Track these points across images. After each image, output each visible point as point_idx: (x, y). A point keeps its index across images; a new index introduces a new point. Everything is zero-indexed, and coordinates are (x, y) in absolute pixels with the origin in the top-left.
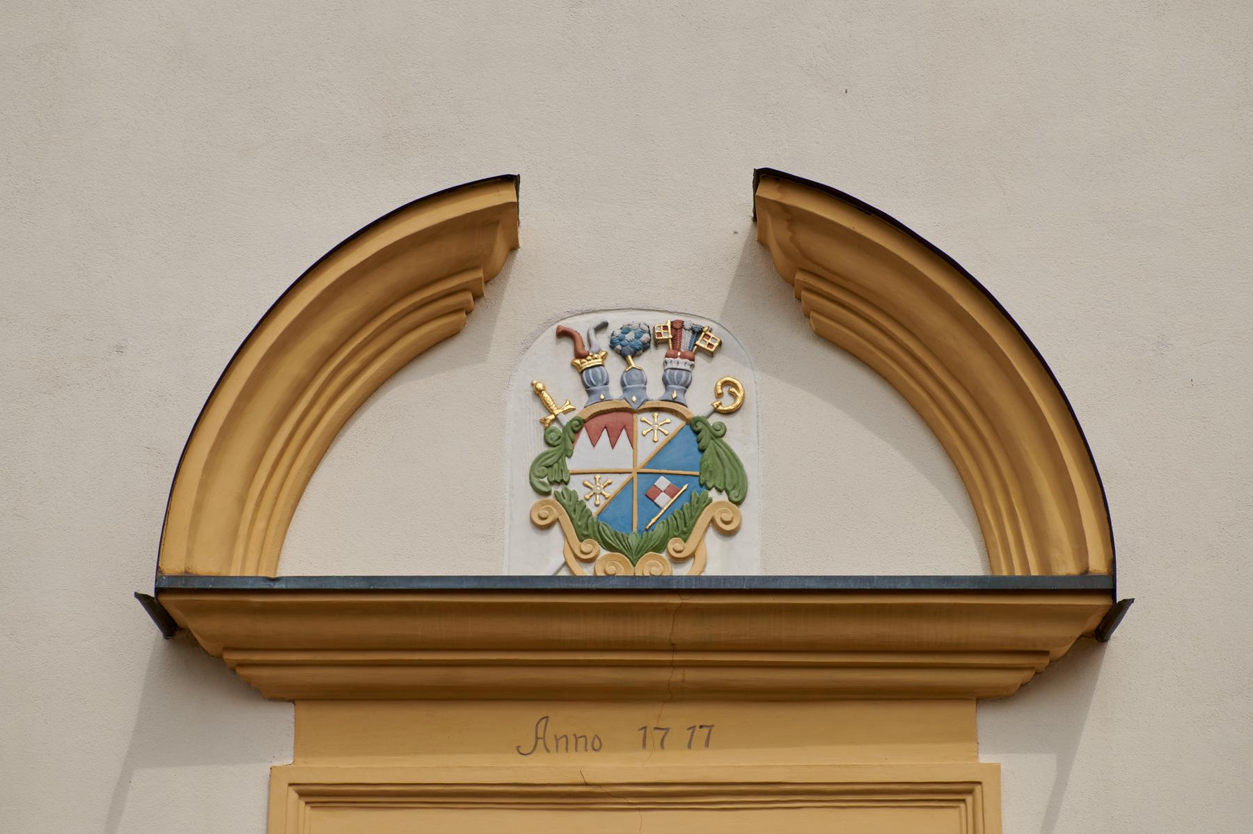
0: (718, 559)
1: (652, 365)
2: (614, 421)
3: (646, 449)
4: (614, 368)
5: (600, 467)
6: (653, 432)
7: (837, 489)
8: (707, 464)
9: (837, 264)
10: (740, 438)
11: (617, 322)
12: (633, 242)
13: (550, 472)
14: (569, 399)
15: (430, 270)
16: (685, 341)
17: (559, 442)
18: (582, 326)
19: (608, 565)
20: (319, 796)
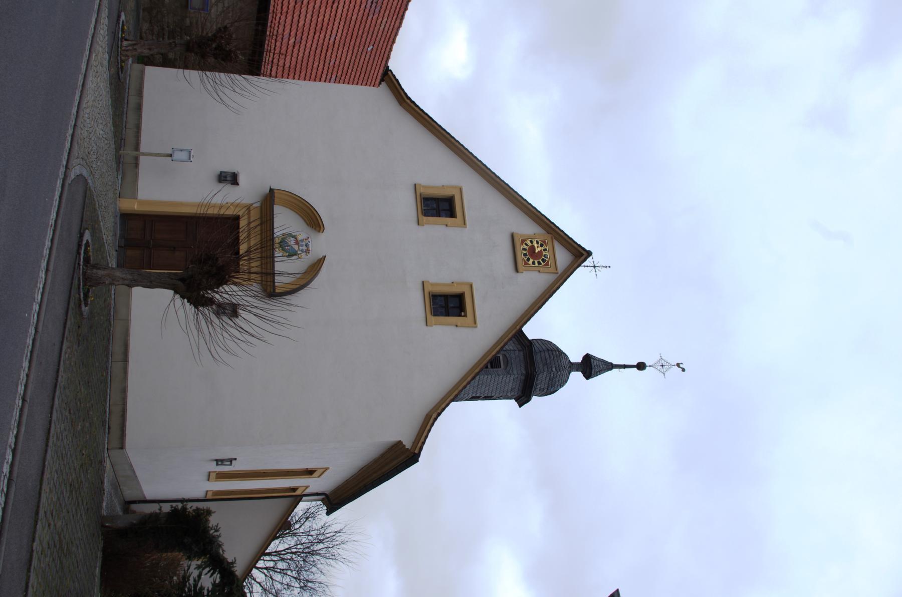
0: (278, 253)
1: (304, 248)
2: (297, 243)
5: (292, 242)
6: (296, 247)
7: (286, 267)
8: (292, 254)
9: (316, 266)
12: (319, 245)
13: (290, 235)
14: (299, 238)
15: (314, 222)
16: (307, 251)
17: (295, 237)
19: (277, 240)
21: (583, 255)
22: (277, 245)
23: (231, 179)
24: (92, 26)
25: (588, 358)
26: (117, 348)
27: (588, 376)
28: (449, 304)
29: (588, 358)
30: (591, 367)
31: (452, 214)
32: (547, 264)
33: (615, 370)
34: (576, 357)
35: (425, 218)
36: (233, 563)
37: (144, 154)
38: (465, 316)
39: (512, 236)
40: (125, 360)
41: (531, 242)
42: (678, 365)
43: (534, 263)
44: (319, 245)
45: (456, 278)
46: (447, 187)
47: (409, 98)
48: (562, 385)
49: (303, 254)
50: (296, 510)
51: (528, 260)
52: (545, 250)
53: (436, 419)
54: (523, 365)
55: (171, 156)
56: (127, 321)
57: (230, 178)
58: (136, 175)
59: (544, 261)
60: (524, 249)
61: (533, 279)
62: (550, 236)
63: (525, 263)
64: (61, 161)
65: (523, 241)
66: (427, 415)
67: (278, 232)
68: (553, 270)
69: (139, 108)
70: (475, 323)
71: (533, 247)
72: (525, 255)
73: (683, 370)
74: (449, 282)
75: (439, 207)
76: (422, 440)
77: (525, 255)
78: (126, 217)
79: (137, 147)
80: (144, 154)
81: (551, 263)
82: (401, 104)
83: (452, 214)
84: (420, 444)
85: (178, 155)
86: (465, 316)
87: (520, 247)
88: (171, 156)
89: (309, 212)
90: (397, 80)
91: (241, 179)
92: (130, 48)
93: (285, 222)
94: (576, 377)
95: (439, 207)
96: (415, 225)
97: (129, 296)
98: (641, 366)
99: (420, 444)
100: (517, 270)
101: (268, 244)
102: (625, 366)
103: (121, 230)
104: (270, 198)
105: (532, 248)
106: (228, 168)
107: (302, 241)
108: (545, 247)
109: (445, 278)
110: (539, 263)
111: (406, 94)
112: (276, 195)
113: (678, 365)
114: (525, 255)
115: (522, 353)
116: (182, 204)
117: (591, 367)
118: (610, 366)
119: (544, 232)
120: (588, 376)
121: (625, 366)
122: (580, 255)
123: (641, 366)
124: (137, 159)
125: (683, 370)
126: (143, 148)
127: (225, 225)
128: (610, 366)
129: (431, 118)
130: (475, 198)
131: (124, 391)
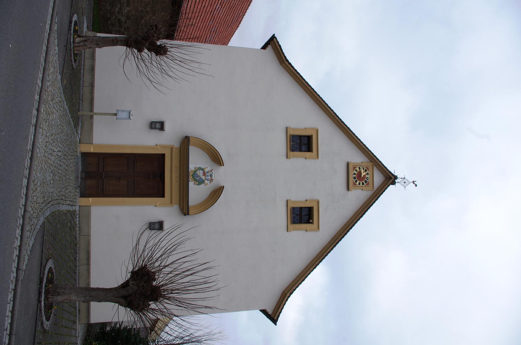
0: (191, 184)
1: (209, 177)
2: (204, 174)
3: (202, 177)
4: (209, 174)
5: (200, 173)
6: (203, 178)
7: (197, 193)
8: (200, 182)
9: (217, 192)
10: (202, 186)
11: (213, 174)
12: (221, 175)
13: (200, 169)
14: (206, 170)
15: (216, 159)
16: (211, 180)
18: (213, 171)
19: (191, 174)
20: (172, 149)
21: (391, 178)
23: (158, 126)
24: (46, 35)
26: (82, 256)
28: (303, 216)
31: (309, 149)
32: (368, 184)
35: (292, 153)
36: (154, 273)
37: (96, 114)
38: (312, 223)
39: (348, 164)
40: (88, 264)
41: (359, 168)
42: (413, 182)
43: (359, 184)
44: (221, 175)
45: (308, 197)
46: (308, 129)
47: (287, 61)
50: (190, 170)
51: (356, 181)
52: (368, 174)
53: (289, 297)
55: (116, 115)
56: (89, 236)
57: (158, 126)
58: (92, 124)
59: (366, 182)
60: (354, 174)
61: (359, 195)
62: (372, 163)
63: (354, 184)
64: (40, 61)
65: (354, 168)
66: (283, 292)
67: (192, 167)
68: (370, 188)
69: (92, 69)
70: (318, 228)
71: (360, 172)
72: (355, 178)
73: (416, 186)
74: (304, 200)
75: (302, 143)
76: (279, 311)
77: (355, 177)
78: (85, 155)
79: (92, 110)
80: (96, 114)
81: (370, 180)
82: (281, 64)
83: (309, 149)
84: (278, 314)
85: (120, 115)
86: (312, 223)
87: (352, 172)
88: (116, 115)
89: (215, 154)
90: (280, 46)
91: (167, 126)
92: (81, 44)
93: (197, 160)
95: (302, 143)
96: (285, 158)
97: (93, 57)
99: (278, 314)
100: (348, 189)
101: (184, 176)
103: (82, 165)
104: (186, 142)
105: (360, 173)
106: (156, 118)
107: (208, 172)
108: (368, 172)
109: (301, 197)
110: (363, 184)
111: (285, 57)
112: (191, 140)
113: (413, 182)
114: (355, 178)
116: (124, 147)
119: (368, 160)
122: (390, 179)
124: (92, 117)
125: (416, 186)
126: (95, 111)
127: (156, 161)
129: (301, 77)
130: (327, 138)
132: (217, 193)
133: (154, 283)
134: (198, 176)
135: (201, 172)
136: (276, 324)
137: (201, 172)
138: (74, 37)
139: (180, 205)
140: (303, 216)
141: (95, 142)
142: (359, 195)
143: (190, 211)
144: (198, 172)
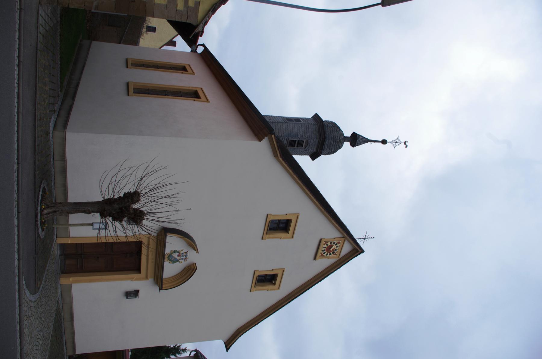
1: (184, 257)
2: (179, 255)
5: (176, 255)
7: (170, 270)
9: (190, 271)
12: (193, 257)
13: (175, 251)
16: (186, 259)
17: (178, 252)
22: (166, 257)
25: (354, 135)
27: (353, 145)
28: (267, 280)
29: (354, 135)
30: (356, 140)
33: (369, 143)
34: (347, 134)
38: (274, 284)
48: (340, 148)
49: (183, 261)
54: (316, 147)
63: (322, 255)
66: (238, 330)
67: (168, 251)
69: (64, 171)
75: (280, 226)
81: (337, 252)
93: (173, 244)
94: (347, 144)
95: (280, 226)
98: (384, 142)
100: (315, 259)
102: (375, 141)
107: (183, 254)
115: (318, 140)
117: (356, 140)
118: (366, 141)
120: (353, 145)
121: (375, 141)
123: (384, 142)
125: (406, 146)
128: (366, 141)
130: (269, 295)
131: (73, 333)
132: (190, 272)
133: (135, 206)
134: (173, 257)
135: (177, 254)
136: (227, 351)
137: (177, 254)
138: (41, 208)
139: (154, 279)
140: (267, 280)
141: (71, 235)
142: (325, 262)
143: (163, 286)
144: (173, 255)
